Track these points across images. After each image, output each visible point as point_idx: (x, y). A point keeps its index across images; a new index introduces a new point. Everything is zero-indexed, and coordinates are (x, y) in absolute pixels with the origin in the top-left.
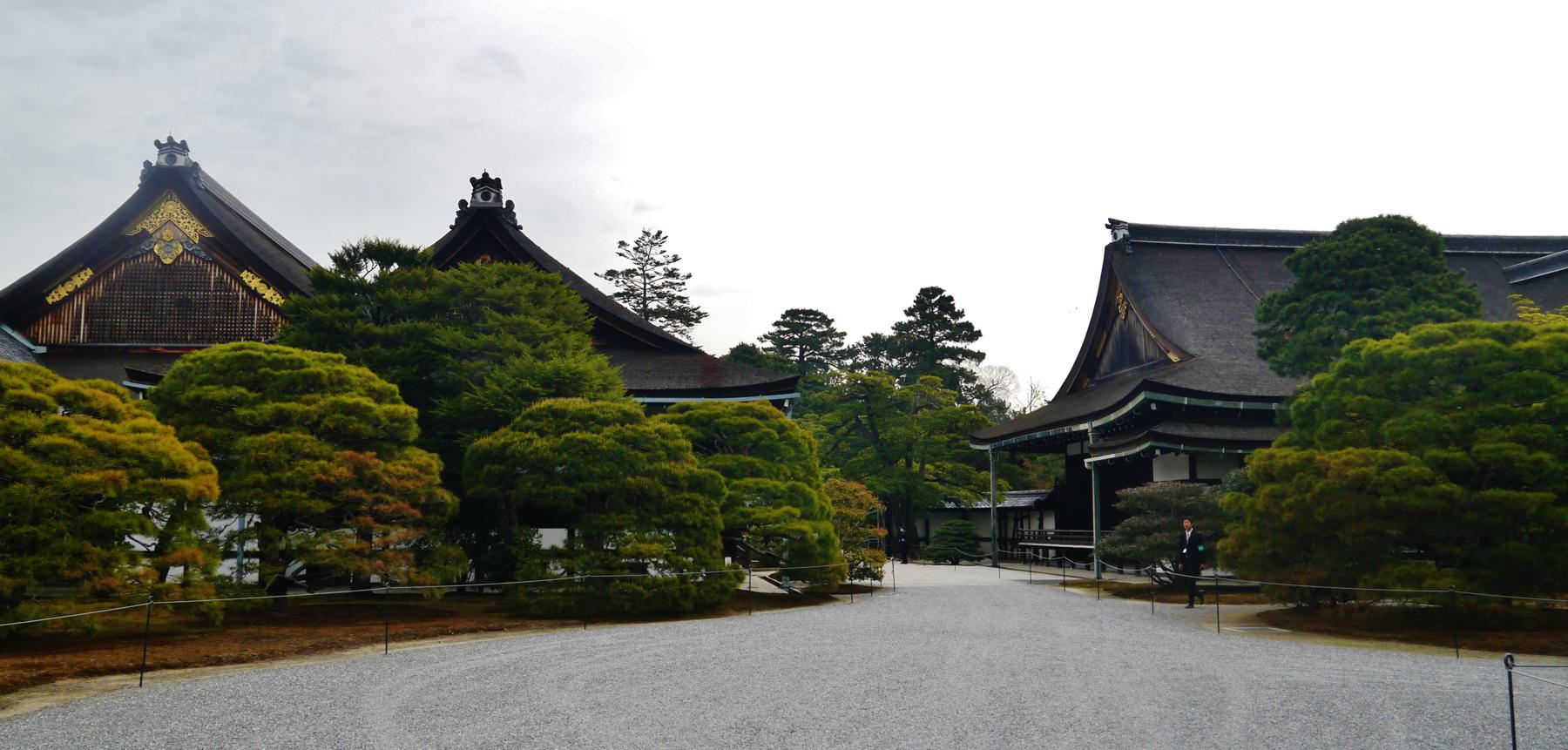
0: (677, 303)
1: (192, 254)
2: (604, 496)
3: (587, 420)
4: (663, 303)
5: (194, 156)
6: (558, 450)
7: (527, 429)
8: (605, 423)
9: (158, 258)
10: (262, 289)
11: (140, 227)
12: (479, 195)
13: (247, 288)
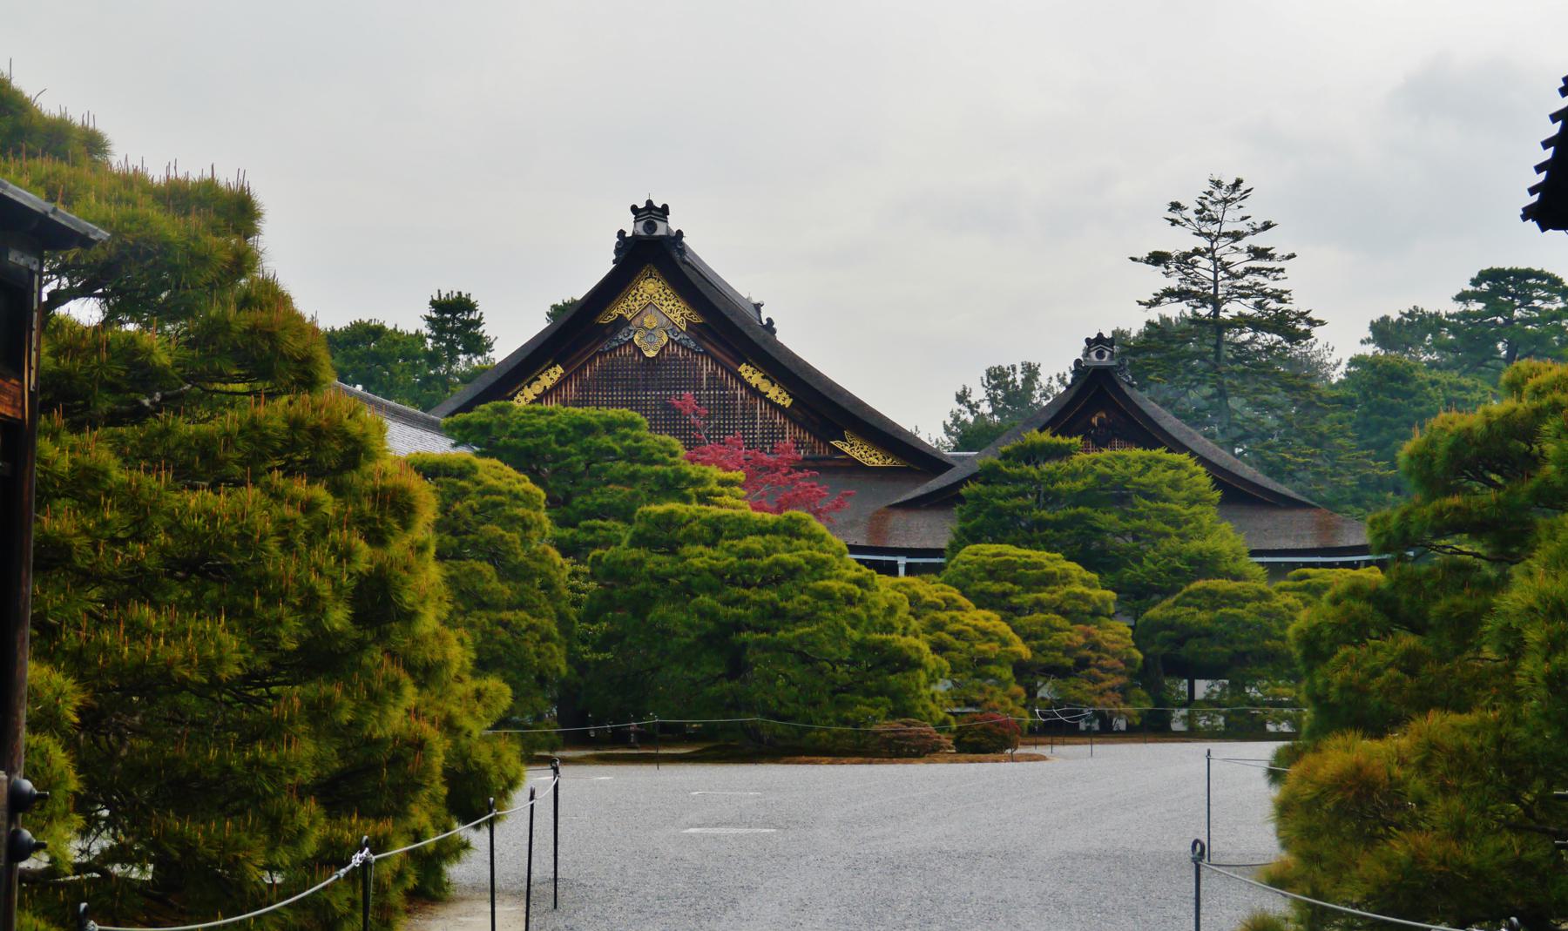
0: (1273, 304)
1: (678, 344)
2: (1244, 654)
3: (1235, 599)
4: (1246, 307)
5: (674, 223)
6: (1216, 621)
7: (1189, 605)
8: (1247, 600)
9: (639, 350)
10: (765, 386)
11: (616, 312)
12: (1093, 354)
13: (747, 386)
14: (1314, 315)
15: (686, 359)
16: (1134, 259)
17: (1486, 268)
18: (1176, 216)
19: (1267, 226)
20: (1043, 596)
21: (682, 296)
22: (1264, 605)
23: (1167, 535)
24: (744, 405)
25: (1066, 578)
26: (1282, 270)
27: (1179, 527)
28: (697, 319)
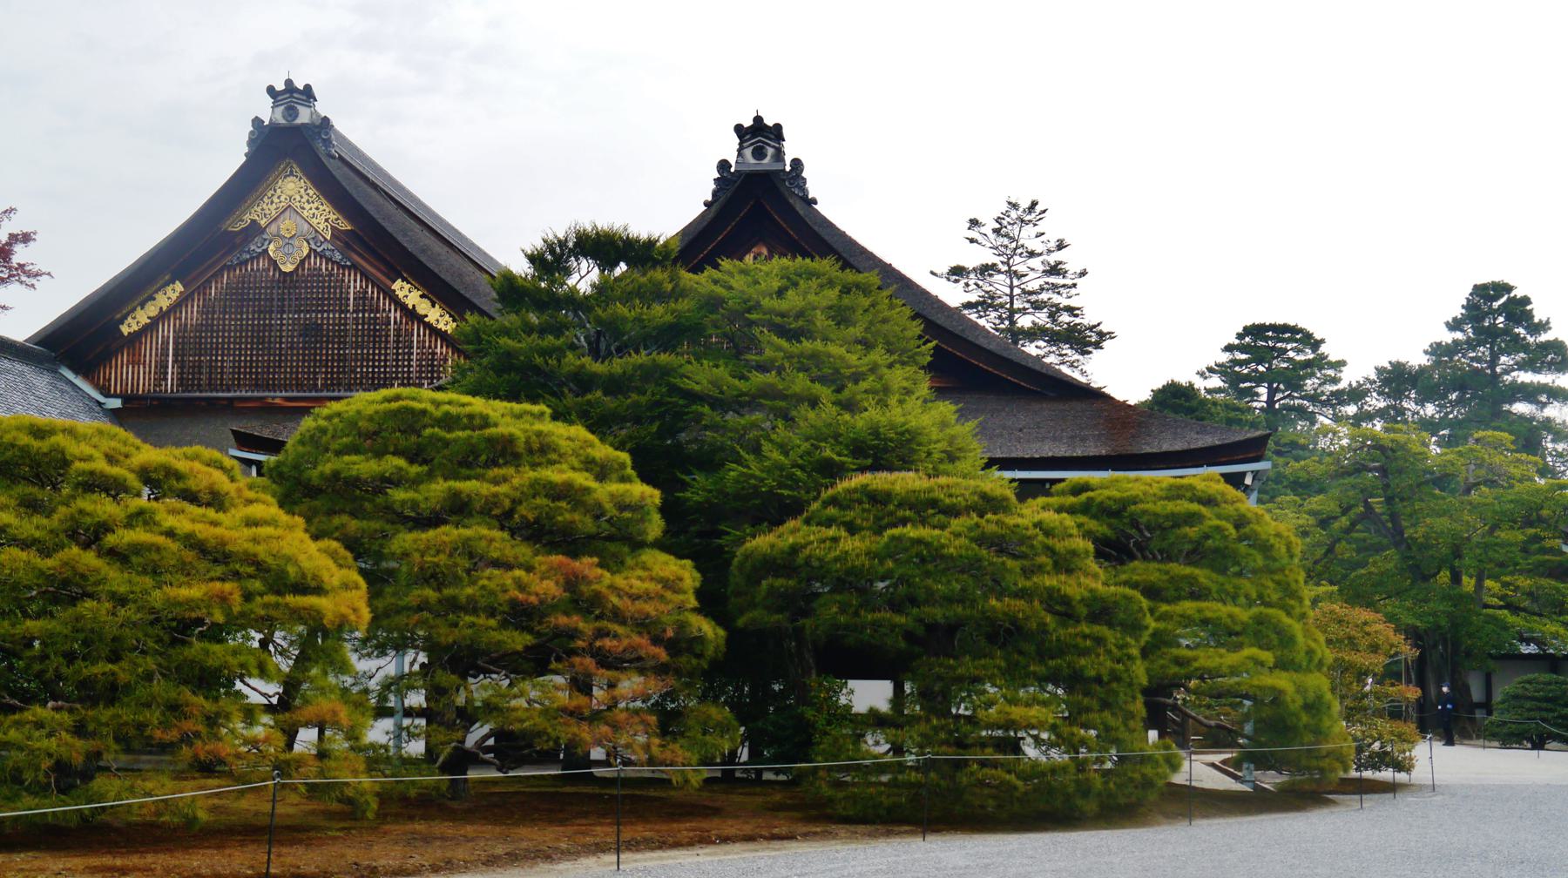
0: (1065, 318)
2: (952, 628)
3: (924, 508)
4: (1042, 318)
5: (323, 108)
7: (829, 522)
8: (953, 512)
9: (274, 263)
10: (423, 307)
11: (247, 218)
12: (748, 152)
13: (402, 307)
14: (1104, 328)
15: (331, 275)
17: (1249, 324)
18: (973, 234)
19: (1061, 246)
20: (468, 486)
21: (326, 197)
22: (990, 523)
23: (814, 403)
24: (398, 330)
25: (543, 451)
26: (1074, 285)
28: (345, 225)
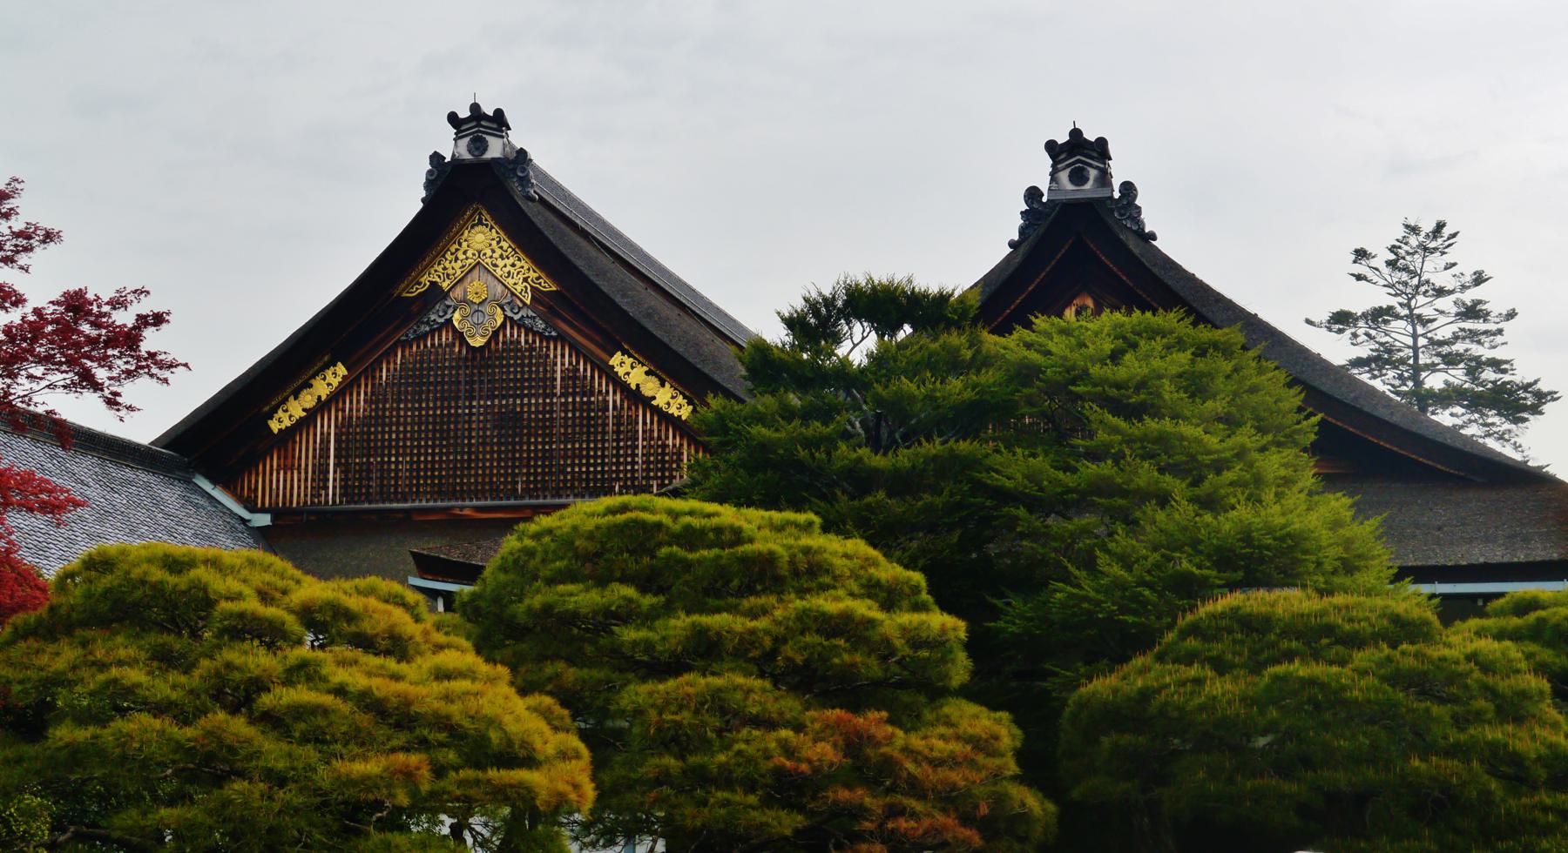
0: (1489, 375)
1: (519, 324)
3: (1316, 637)
4: (1457, 376)
7: (1190, 659)
8: (1355, 641)
9: (459, 336)
10: (650, 387)
11: (426, 280)
12: (1064, 176)
14: (1543, 387)
16: (1308, 322)
18: (1360, 269)
19: (1479, 279)
22: (1406, 655)
23: (1164, 500)
24: (618, 418)
25: (812, 573)
26: (1500, 332)
27: (1196, 483)
28: (548, 286)
